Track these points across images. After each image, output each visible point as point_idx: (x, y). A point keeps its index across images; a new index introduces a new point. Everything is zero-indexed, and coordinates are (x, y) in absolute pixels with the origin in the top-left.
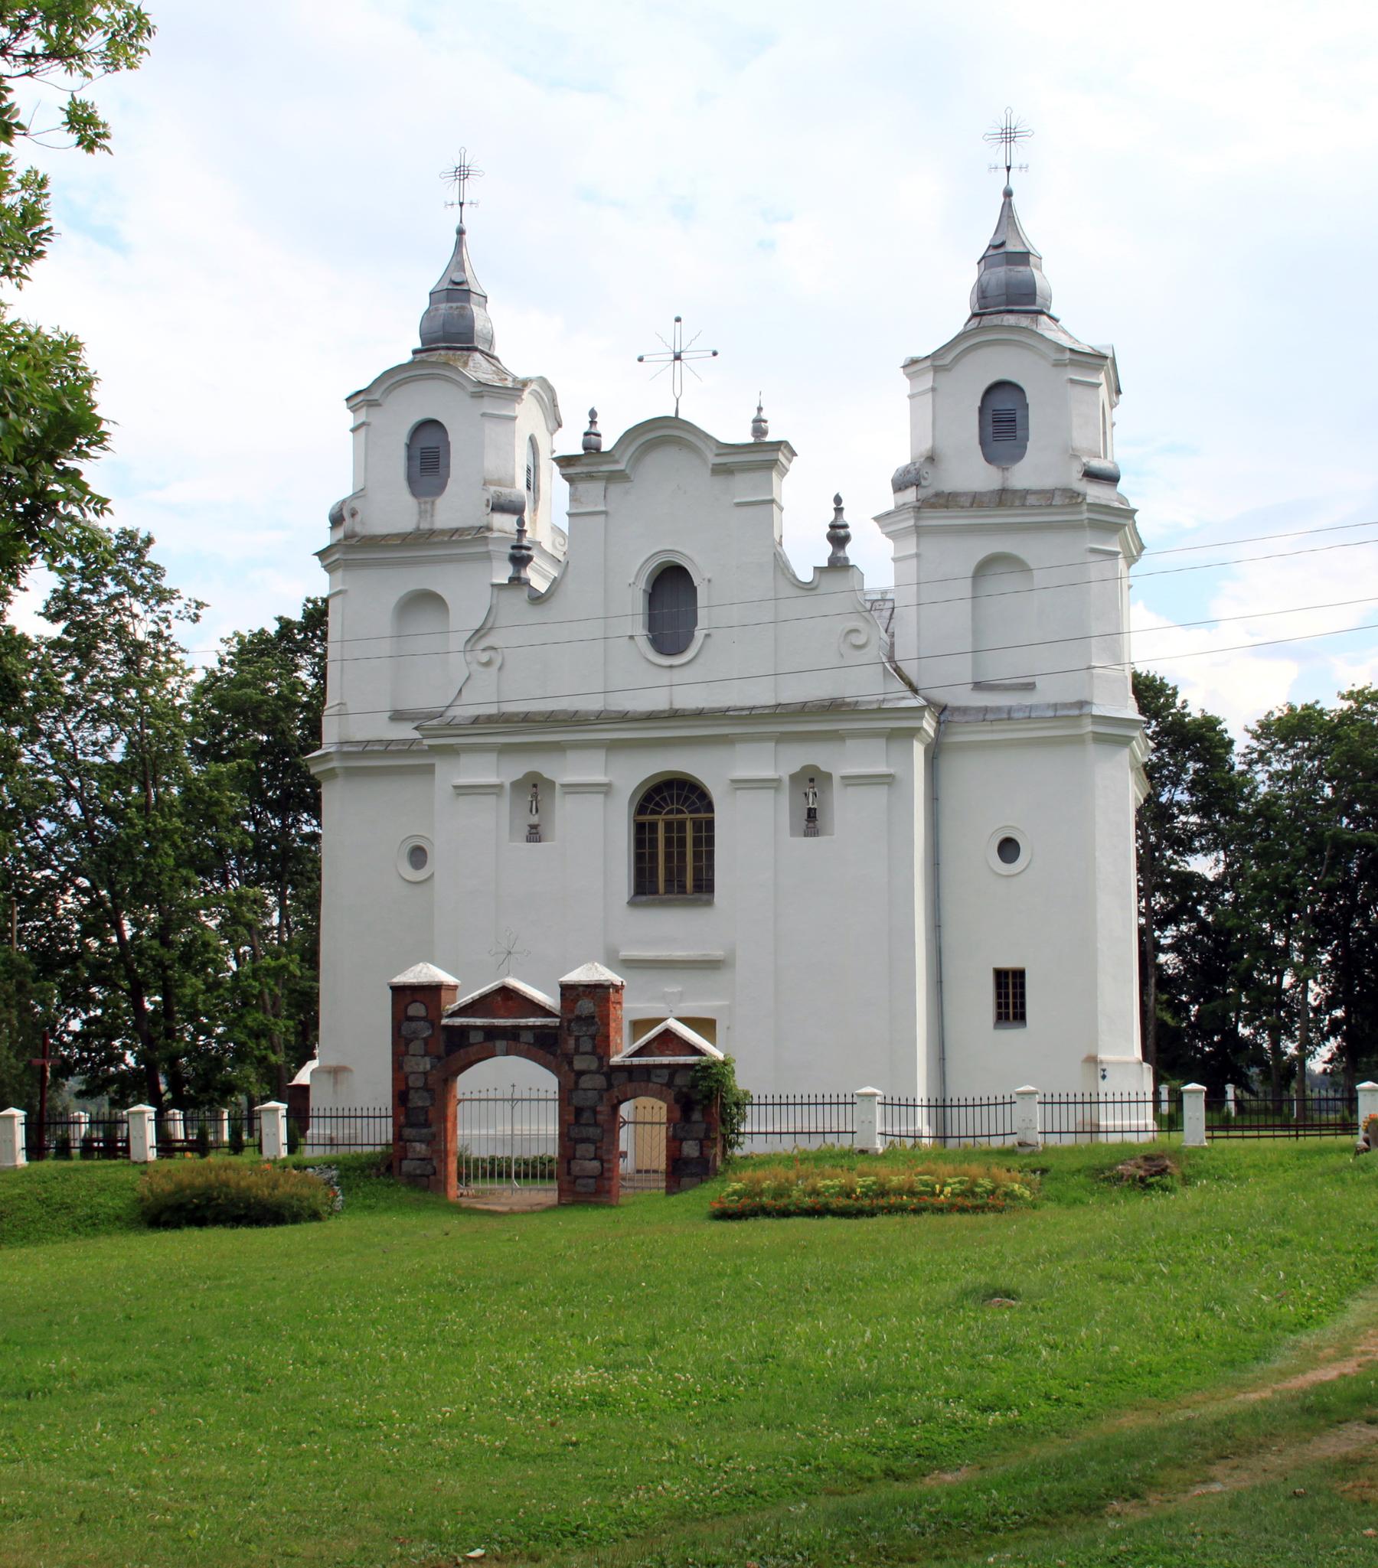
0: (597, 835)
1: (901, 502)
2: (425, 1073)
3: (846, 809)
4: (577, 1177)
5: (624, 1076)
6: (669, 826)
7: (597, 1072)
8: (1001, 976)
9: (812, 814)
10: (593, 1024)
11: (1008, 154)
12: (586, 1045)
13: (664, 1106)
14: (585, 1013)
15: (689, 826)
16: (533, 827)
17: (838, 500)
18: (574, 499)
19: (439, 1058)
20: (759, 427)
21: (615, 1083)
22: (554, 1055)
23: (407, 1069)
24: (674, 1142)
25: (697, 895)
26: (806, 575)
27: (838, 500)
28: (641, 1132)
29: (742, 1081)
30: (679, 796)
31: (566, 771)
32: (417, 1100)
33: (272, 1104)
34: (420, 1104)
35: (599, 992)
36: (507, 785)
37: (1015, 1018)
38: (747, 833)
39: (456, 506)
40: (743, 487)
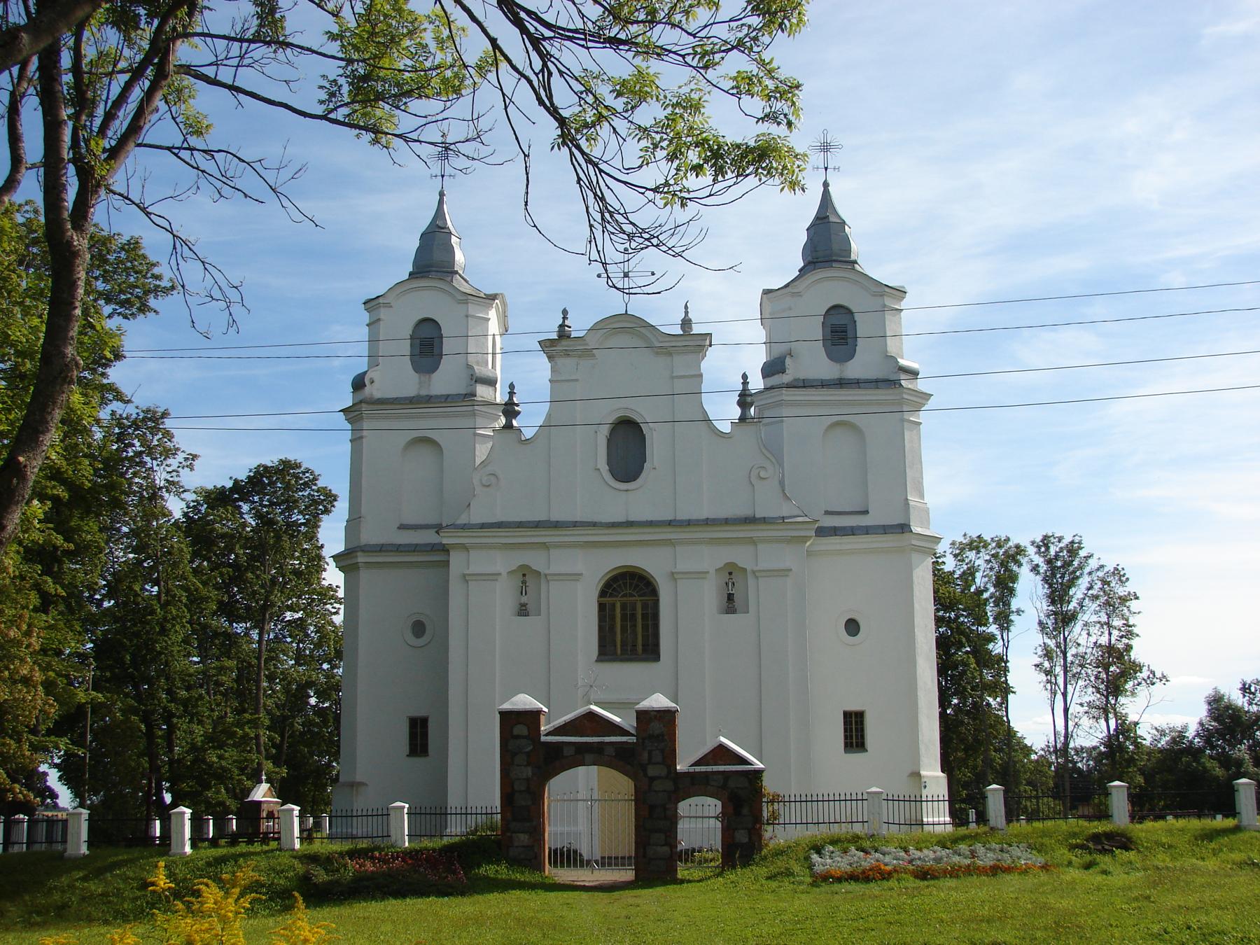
0: (577, 613)
2: (528, 780)
6: (624, 607)
8: (847, 715)
9: (730, 597)
11: (826, 160)
13: (719, 803)
16: (523, 605)
20: (686, 323)
24: (727, 832)
26: (725, 427)
28: (699, 822)
29: (770, 785)
30: (631, 584)
31: (561, 562)
35: (666, 717)
36: (504, 572)
38: (687, 612)
39: (445, 380)
40: (680, 364)
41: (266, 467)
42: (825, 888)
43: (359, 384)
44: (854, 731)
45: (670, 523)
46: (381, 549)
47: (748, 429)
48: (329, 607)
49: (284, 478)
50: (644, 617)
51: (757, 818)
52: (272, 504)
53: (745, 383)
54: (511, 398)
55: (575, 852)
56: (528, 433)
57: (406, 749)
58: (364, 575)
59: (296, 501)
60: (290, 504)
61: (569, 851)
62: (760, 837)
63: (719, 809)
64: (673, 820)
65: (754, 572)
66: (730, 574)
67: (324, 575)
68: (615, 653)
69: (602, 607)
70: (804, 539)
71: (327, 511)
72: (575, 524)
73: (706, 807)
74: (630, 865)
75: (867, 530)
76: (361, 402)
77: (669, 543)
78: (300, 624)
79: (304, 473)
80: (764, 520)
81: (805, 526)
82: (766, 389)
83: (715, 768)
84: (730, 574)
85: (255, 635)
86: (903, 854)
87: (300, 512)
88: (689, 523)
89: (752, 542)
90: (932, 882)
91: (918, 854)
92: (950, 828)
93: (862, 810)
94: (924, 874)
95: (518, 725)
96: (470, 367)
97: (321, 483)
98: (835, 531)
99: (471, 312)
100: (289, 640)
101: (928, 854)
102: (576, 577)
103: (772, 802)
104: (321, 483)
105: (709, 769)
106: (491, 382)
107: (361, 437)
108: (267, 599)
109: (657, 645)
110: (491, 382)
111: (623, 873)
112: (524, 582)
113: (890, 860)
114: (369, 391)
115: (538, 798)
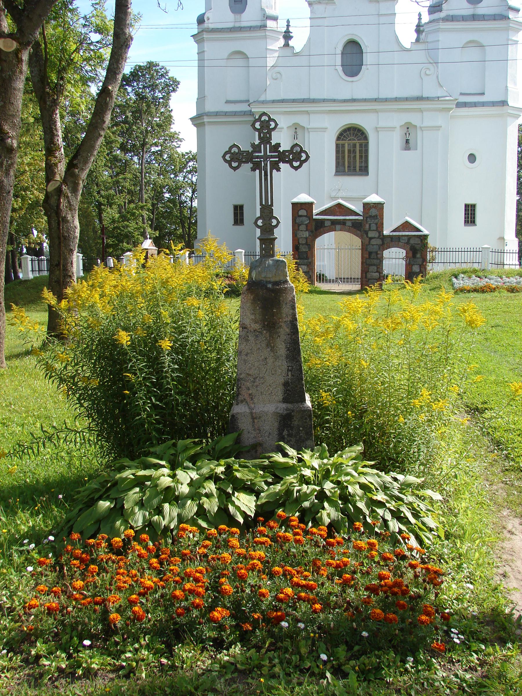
1: (432, 19)
2: (306, 238)
3: (423, 139)
4: (369, 279)
5: (389, 240)
7: (378, 238)
9: (407, 141)
10: (377, 219)
12: (374, 227)
14: (373, 214)
15: (346, 145)
17: (288, 22)
18: (312, 12)
19: (312, 232)
21: (386, 242)
22: (360, 231)
23: (298, 236)
24: (409, 266)
25: (360, 173)
26: (408, 46)
27: (288, 22)
28: (394, 260)
29: (431, 243)
31: (316, 121)
32: (303, 249)
33: (239, 250)
34: (304, 250)
35: (379, 206)
37: (471, 222)
38: (383, 149)
39: (249, 17)
41: (140, 66)
42: (462, 295)
43: (201, 20)
44: (470, 214)
45: (375, 100)
46: (217, 114)
47: (421, 46)
48: (174, 144)
49: (150, 72)
50: (360, 151)
51: (424, 260)
52: (144, 87)
53: (420, 19)
54: (288, 29)
55: (323, 275)
56: (298, 49)
57: (232, 221)
58: (208, 129)
59: (157, 85)
60: (153, 87)
61: (320, 275)
62: (425, 269)
63: (404, 254)
64: (381, 260)
65: (421, 128)
66: (408, 128)
67: (172, 126)
68: (344, 171)
69: (337, 146)
70: (449, 109)
71: (174, 90)
72: (324, 100)
73: (397, 253)
74: (358, 282)
75: (483, 104)
76: (203, 31)
77: (376, 111)
78: (160, 153)
79: (161, 69)
80: (428, 99)
81: (449, 102)
82: (430, 22)
83: (404, 233)
84: (408, 128)
85: (136, 159)
86: (500, 279)
87: (160, 92)
88: (386, 100)
89: (421, 111)
90: (517, 294)
91: (507, 280)
92: (518, 267)
93: (478, 257)
94: (512, 290)
95: (301, 210)
96: (263, 10)
97: (170, 75)
98: (465, 105)
99: (510, 38)
100: (154, 162)
101: (513, 280)
102: (324, 129)
103: (432, 251)
104: (170, 75)
105: (401, 233)
106: (275, 19)
107: (204, 52)
108: (144, 140)
109: (367, 167)
110: (275, 19)
111: (351, 286)
112: (296, 132)
113: (493, 283)
114: (208, 25)
115: (311, 247)
